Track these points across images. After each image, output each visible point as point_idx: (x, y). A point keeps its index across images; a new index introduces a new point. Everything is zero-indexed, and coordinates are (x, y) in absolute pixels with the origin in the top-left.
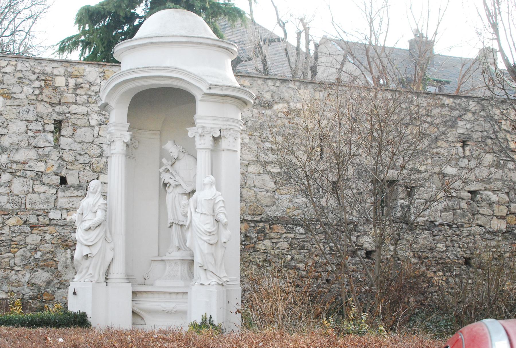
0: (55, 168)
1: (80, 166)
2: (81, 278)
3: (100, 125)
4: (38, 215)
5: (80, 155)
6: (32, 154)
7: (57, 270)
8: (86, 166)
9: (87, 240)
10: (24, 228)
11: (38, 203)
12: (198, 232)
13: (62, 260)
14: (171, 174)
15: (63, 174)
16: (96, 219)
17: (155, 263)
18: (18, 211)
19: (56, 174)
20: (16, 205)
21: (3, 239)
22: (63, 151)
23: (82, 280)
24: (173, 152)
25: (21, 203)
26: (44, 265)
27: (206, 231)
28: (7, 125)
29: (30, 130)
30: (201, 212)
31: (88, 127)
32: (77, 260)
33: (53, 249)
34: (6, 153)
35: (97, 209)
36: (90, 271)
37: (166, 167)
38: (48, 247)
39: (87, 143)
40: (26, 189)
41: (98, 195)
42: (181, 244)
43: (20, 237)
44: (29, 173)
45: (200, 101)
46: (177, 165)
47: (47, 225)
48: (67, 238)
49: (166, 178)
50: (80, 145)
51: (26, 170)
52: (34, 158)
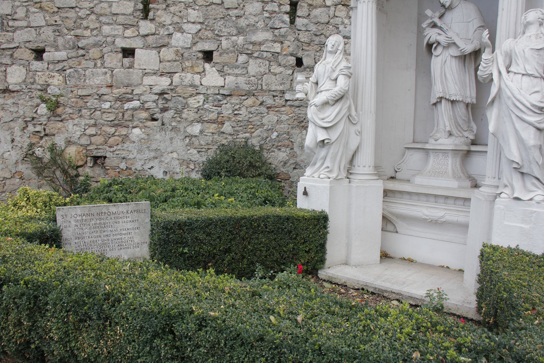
0: (291, 49)
1: (316, 46)
2: (314, 173)
3: (336, 5)
4: (274, 96)
6: (268, 35)
7: (293, 150)
9: (323, 119)
10: (261, 108)
11: (274, 84)
12: (518, 108)
13: (298, 140)
14: (440, 28)
15: (299, 55)
16: (337, 89)
17: (408, 153)
18: (254, 92)
19: (292, 55)
20: (253, 86)
21: (240, 119)
22: (299, 32)
23: (316, 175)
25: (258, 84)
26: (281, 146)
27: (533, 105)
28: (244, 6)
29: (266, 11)
30: (524, 73)
31: (324, 7)
32: (308, 148)
33: (289, 130)
34: (242, 34)
35: (338, 75)
36: (328, 163)
37: (431, 21)
38: (284, 127)
39: (323, 24)
40: (262, 70)
41: (339, 56)
42: (452, 127)
43: (257, 118)
44: (265, 54)
46: (449, 16)
47: (284, 106)
48: (302, 119)
49: (432, 35)
50: (316, 26)
51: (262, 51)
52: (270, 39)
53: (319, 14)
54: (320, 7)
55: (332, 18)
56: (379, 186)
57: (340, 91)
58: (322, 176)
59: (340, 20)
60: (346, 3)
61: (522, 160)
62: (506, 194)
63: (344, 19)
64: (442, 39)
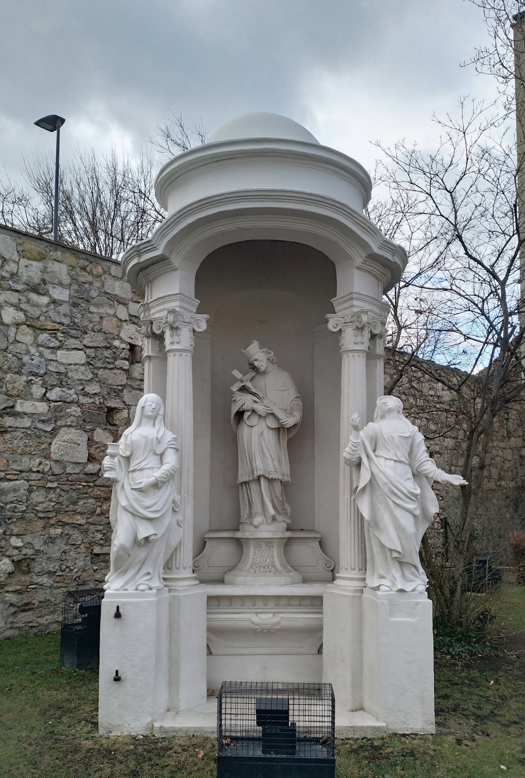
24: (260, 359)
35: (166, 449)
45: (358, 268)
57: (173, 470)
58: (142, 587)
59: (24, 347)
60: (34, 324)
61: (403, 549)
62: (387, 586)
63: (30, 348)
64: (260, 408)
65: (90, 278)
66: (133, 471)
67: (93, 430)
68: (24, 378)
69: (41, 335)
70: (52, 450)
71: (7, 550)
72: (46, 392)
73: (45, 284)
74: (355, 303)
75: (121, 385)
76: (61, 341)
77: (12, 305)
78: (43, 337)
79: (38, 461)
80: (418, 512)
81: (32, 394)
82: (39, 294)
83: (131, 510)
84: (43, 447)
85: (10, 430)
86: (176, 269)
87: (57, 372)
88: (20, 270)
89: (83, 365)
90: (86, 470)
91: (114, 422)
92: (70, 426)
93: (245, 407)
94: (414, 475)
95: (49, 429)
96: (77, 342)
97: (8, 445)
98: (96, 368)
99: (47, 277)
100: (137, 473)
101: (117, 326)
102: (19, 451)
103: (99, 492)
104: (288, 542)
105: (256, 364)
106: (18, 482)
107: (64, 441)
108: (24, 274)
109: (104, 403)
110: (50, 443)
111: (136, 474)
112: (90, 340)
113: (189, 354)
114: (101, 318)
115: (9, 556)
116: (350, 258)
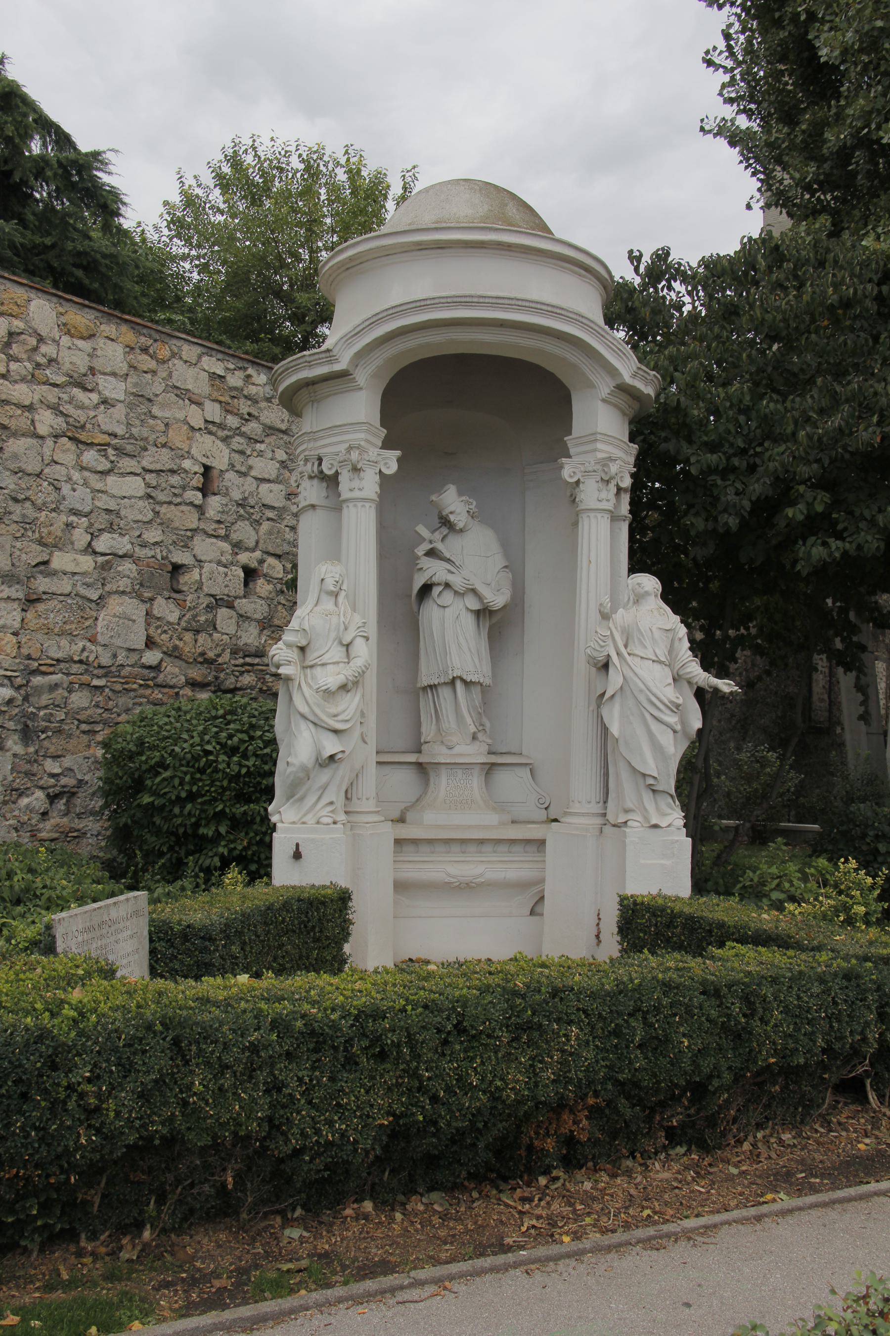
1: (14, 526)
2: (305, 815)
3: (56, 437)
5: (16, 500)
8: (25, 529)
9: (335, 716)
23: (310, 819)
24: (458, 511)
27: (671, 702)
39: (29, 475)
45: (604, 401)
49: (434, 570)
50: (15, 478)
53: (22, 451)
54: (23, 435)
55: (48, 465)
56: (389, 832)
63: (72, 472)
64: (456, 581)
65: (153, 364)
66: (312, 667)
67: (152, 599)
68: (63, 518)
69: (86, 453)
70: (99, 629)
71: (41, 778)
72: (92, 539)
73: (94, 375)
74: (599, 446)
75: (190, 530)
76: (112, 462)
77: (49, 407)
78: (90, 457)
79: (81, 645)
80: (678, 727)
81: (72, 543)
82: (85, 389)
83: (312, 718)
84: (87, 623)
85: (44, 597)
86: (361, 389)
87: (106, 510)
88: (60, 354)
89: (140, 498)
90: (144, 660)
91: (180, 587)
92: (123, 592)
93: (435, 579)
94: (674, 680)
95: (95, 597)
96: (133, 462)
97: (42, 620)
98: (158, 503)
99: (98, 364)
100: (319, 669)
101: (188, 438)
102: (56, 630)
103: (160, 696)
104: (490, 769)
105: (452, 518)
106: (54, 677)
107: (115, 616)
108: (67, 359)
109: (167, 557)
110: (96, 619)
111: (318, 671)
112: (151, 459)
113: (374, 506)
114: (167, 425)
115: (42, 788)
116: (591, 386)
